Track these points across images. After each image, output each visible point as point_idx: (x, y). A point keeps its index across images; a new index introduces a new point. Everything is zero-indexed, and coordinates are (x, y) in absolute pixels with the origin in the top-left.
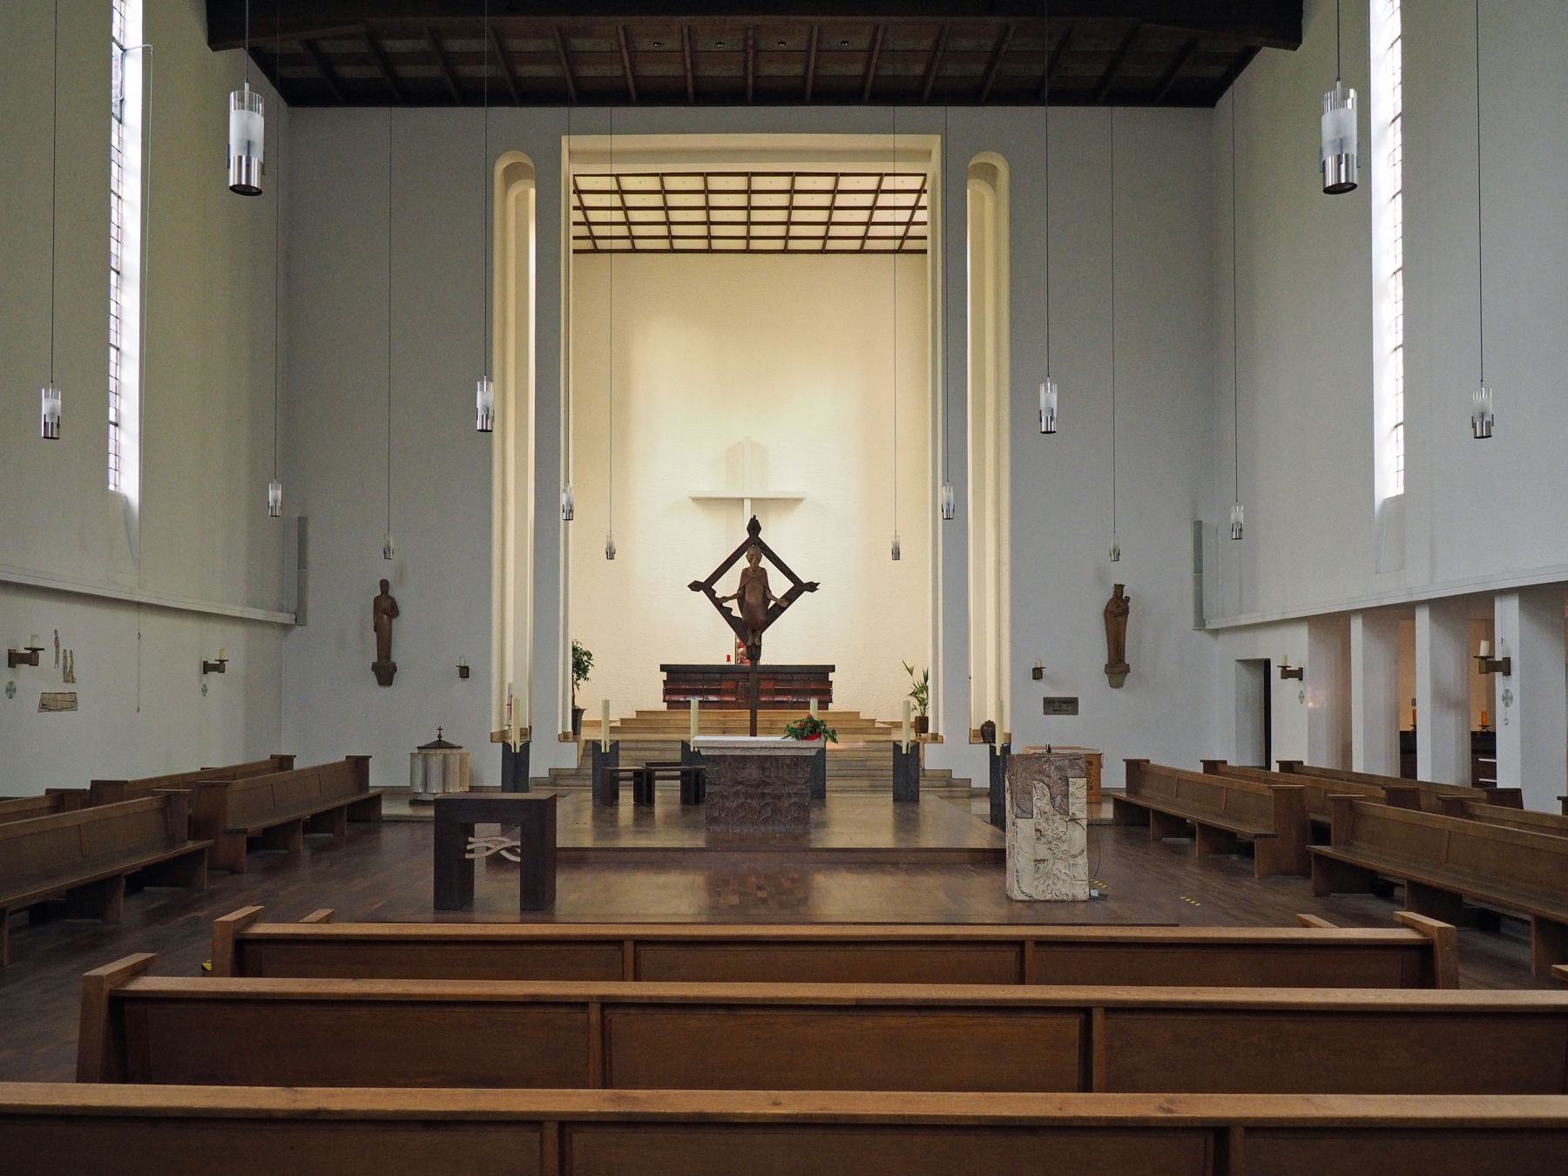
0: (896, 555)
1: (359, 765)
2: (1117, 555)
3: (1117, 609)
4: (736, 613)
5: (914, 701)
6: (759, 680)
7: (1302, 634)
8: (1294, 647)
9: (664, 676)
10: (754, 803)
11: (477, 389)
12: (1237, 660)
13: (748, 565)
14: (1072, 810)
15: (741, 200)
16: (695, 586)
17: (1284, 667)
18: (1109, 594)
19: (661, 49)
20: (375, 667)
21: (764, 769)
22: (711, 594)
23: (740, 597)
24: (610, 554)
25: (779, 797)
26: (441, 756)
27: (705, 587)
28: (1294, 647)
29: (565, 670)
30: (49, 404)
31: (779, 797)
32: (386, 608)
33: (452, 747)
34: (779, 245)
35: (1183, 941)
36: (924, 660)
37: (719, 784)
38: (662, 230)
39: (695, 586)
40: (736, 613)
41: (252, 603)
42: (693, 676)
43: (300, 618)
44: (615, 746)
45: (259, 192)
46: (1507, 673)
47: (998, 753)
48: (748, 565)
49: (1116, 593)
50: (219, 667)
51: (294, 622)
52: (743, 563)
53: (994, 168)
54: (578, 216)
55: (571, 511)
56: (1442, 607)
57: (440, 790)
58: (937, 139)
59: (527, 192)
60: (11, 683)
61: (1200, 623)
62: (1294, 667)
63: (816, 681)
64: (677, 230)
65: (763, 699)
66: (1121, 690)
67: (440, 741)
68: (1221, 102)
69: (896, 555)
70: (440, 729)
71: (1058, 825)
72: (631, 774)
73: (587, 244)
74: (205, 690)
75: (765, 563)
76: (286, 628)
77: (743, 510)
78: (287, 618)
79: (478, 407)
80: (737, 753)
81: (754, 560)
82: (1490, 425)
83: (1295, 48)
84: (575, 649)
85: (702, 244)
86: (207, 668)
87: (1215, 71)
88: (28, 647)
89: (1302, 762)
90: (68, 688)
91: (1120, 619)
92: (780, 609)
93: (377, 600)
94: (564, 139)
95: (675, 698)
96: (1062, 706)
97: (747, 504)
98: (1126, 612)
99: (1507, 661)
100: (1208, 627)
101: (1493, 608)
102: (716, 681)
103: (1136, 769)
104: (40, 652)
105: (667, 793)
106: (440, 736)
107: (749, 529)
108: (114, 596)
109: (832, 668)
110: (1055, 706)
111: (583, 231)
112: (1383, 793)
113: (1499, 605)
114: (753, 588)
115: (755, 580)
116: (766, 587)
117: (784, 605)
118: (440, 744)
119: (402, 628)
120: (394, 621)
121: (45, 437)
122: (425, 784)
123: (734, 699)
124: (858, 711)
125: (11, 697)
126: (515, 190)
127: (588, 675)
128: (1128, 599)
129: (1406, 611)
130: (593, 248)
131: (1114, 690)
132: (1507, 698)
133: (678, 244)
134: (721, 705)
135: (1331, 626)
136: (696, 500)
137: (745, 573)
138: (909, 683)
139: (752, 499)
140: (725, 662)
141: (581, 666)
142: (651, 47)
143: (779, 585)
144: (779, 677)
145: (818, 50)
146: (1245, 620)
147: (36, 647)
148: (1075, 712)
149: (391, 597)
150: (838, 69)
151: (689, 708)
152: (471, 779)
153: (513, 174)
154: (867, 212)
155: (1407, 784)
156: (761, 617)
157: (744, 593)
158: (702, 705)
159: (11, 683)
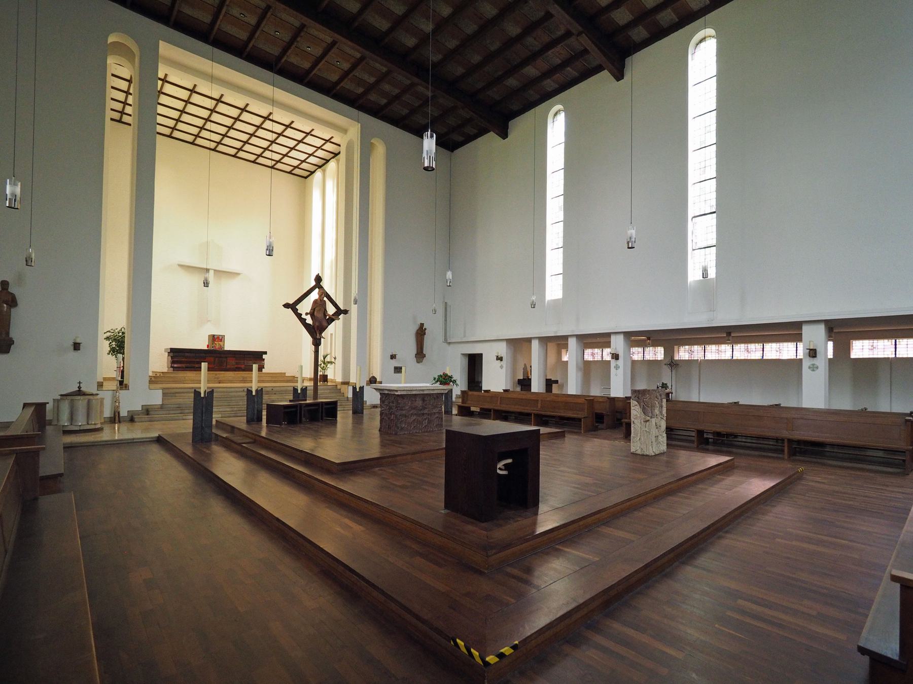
3: (421, 333)
4: (309, 321)
7: (504, 344)
11: (7, 184)
12: (462, 354)
16: (287, 306)
17: (497, 356)
18: (417, 327)
19: (243, 19)
22: (295, 311)
23: (312, 314)
26: (86, 400)
27: (292, 307)
37: (405, 410)
39: (287, 306)
47: (358, 390)
52: (315, 295)
61: (446, 341)
67: (79, 390)
68: (457, 152)
70: (80, 383)
87: (461, 139)
92: (331, 320)
95: (175, 366)
100: (448, 341)
106: (79, 387)
109: (265, 353)
113: (613, 338)
114: (320, 310)
118: (80, 393)
124: (285, 372)
125: (809, 368)
128: (425, 329)
137: (315, 302)
139: (215, 270)
142: (237, 15)
143: (331, 310)
151: (201, 371)
155: (525, 395)
157: (314, 312)
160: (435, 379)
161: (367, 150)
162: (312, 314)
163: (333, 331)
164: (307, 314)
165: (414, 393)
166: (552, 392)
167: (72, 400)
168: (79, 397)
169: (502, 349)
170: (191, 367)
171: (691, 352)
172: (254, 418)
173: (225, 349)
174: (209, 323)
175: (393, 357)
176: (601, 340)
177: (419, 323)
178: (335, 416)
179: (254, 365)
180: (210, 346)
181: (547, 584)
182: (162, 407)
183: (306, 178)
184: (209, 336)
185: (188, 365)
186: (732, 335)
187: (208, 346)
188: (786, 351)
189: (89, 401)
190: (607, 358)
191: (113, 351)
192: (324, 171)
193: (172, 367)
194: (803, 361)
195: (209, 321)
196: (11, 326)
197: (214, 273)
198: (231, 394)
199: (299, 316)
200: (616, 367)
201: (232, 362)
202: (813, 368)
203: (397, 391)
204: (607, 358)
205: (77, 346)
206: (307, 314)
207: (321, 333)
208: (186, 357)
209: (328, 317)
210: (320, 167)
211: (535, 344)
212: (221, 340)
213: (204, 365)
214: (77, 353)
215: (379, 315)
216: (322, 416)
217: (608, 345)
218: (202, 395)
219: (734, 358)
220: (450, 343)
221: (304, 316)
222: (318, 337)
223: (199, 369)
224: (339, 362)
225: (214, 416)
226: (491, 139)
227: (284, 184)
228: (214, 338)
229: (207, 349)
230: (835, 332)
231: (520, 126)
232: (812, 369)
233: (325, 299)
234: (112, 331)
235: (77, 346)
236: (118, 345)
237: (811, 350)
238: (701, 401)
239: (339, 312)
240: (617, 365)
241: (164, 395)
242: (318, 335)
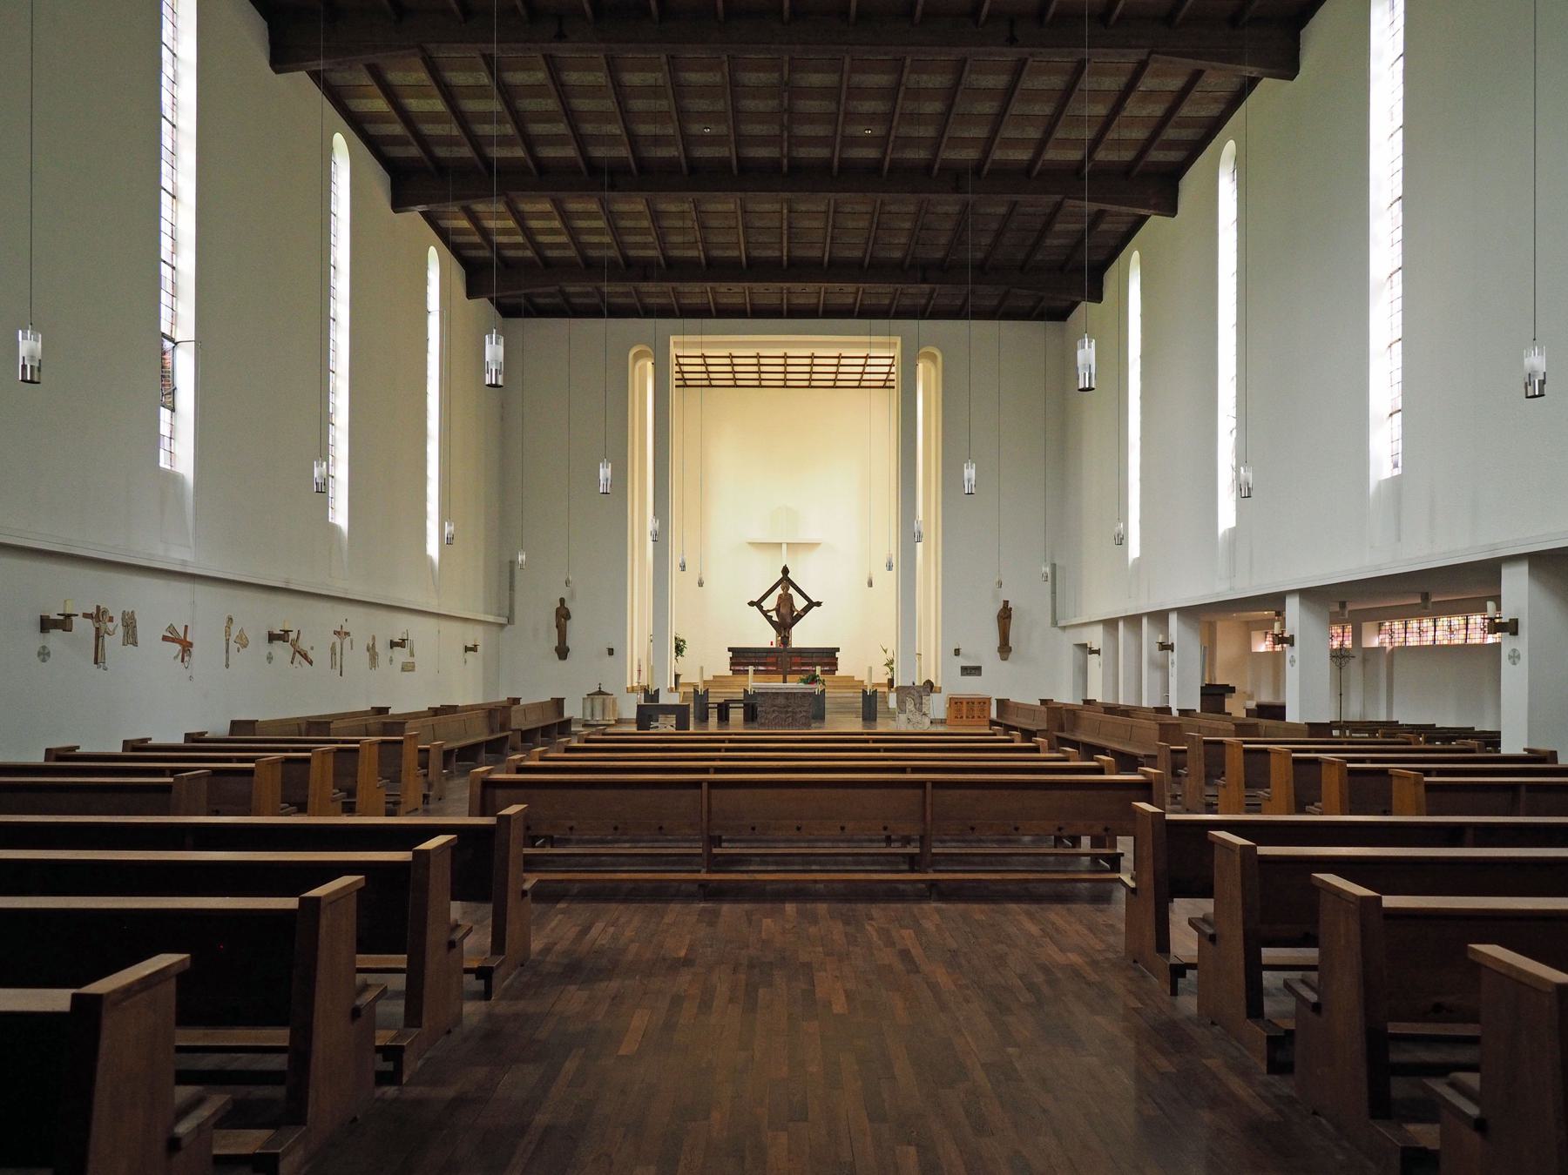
0: (870, 584)
1: (558, 703)
2: (1000, 584)
3: (1005, 615)
4: (775, 618)
5: (888, 669)
6: (791, 657)
7: (1099, 629)
8: (1096, 637)
9: (730, 654)
10: (783, 716)
13: (782, 592)
15: (781, 369)
16: (752, 604)
20: (557, 649)
21: (787, 699)
22: (761, 608)
23: (777, 610)
24: (701, 584)
25: (796, 713)
27: (757, 604)
28: (1096, 637)
29: (671, 650)
30: (28, 346)
31: (796, 713)
32: (563, 615)
33: (608, 694)
34: (806, 383)
36: (891, 645)
38: (730, 376)
39: (752, 604)
40: (775, 618)
41: (486, 613)
42: (750, 654)
43: (510, 620)
44: (707, 691)
45: (501, 386)
48: (782, 592)
50: (474, 649)
51: (506, 622)
52: (779, 591)
53: (935, 356)
54: (677, 369)
55: (684, 566)
56: (1151, 615)
57: (601, 718)
58: (900, 338)
59: (645, 365)
60: (44, 647)
61: (1055, 623)
62: (1096, 648)
63: (828, 657)
64: (738, 376)
65: (793, 668)
69: (870, 584)
72: (716, 705)
73: (681, 383)
74: (270, 658)
75: (791, 591)
76: (502, 626)
78: (503, 620)
79: (601, 478)
80: (774, 691)
81: (785, 589)
82: (1542, 383)
83: (1292, 79)
84: (676, 638)
85: (756, 383)
86: (467, 649)
87: (1174, 156)
88: (62, 612)
89: (1195, 710)
90: (411, 660)
91: (1006, 620)
92: (799, 617)
93: (558, 610)
94: (671, 337)
95: (737, 668)
96: (971, 671)
97: (784, 546)
98: (1009, 617)
99: (1292, 636)
102: (763, 657)
103: (1002, 704)
104: (73, 618)
105: (737, 715)
106: (600, 688)
108: (379, 602)
109: (838, 650)
110: (966, 671)
111: (679, 376)
112: (1233, 727)
114: (785, 605)
115: (786, 600)
116: (792, 605)
117: (802, 614)
118: (600, 693)
119: (573, 627)
120: (568, 622)
121: (22, 380)
122: (592, 715)
123: (775, 668)
125: (44, 661)
126: (640, 363)
127: (683, 654)
130: (684, 384)
133: (739, 383)
134: (767, 672)
135: (1110, 624)
136: (750, 543)
137: (780, 597)
138: (884, 659)
140: (769, 646)
141: (679, 649)
143: (799, 603)
144: (803, 655)
145: (835, 212)
146: (1075, 621)
147: (68, 612)
148: (980, 674)
149: (567, 609)
150: (847, 254)
152: (619, 714)
153: (637, 357)
154: (864, 360)
156: (789, 620)
158: (756, 672)
159: (270, 653)
166: (1284, 719)
167: (592, 699)
181: (765, 837)
186: (1434, 600)
205: (611, 652)
209: (796, 613)
219: (1437, 643)
220: (1064, 628)
230: (1435, 602)
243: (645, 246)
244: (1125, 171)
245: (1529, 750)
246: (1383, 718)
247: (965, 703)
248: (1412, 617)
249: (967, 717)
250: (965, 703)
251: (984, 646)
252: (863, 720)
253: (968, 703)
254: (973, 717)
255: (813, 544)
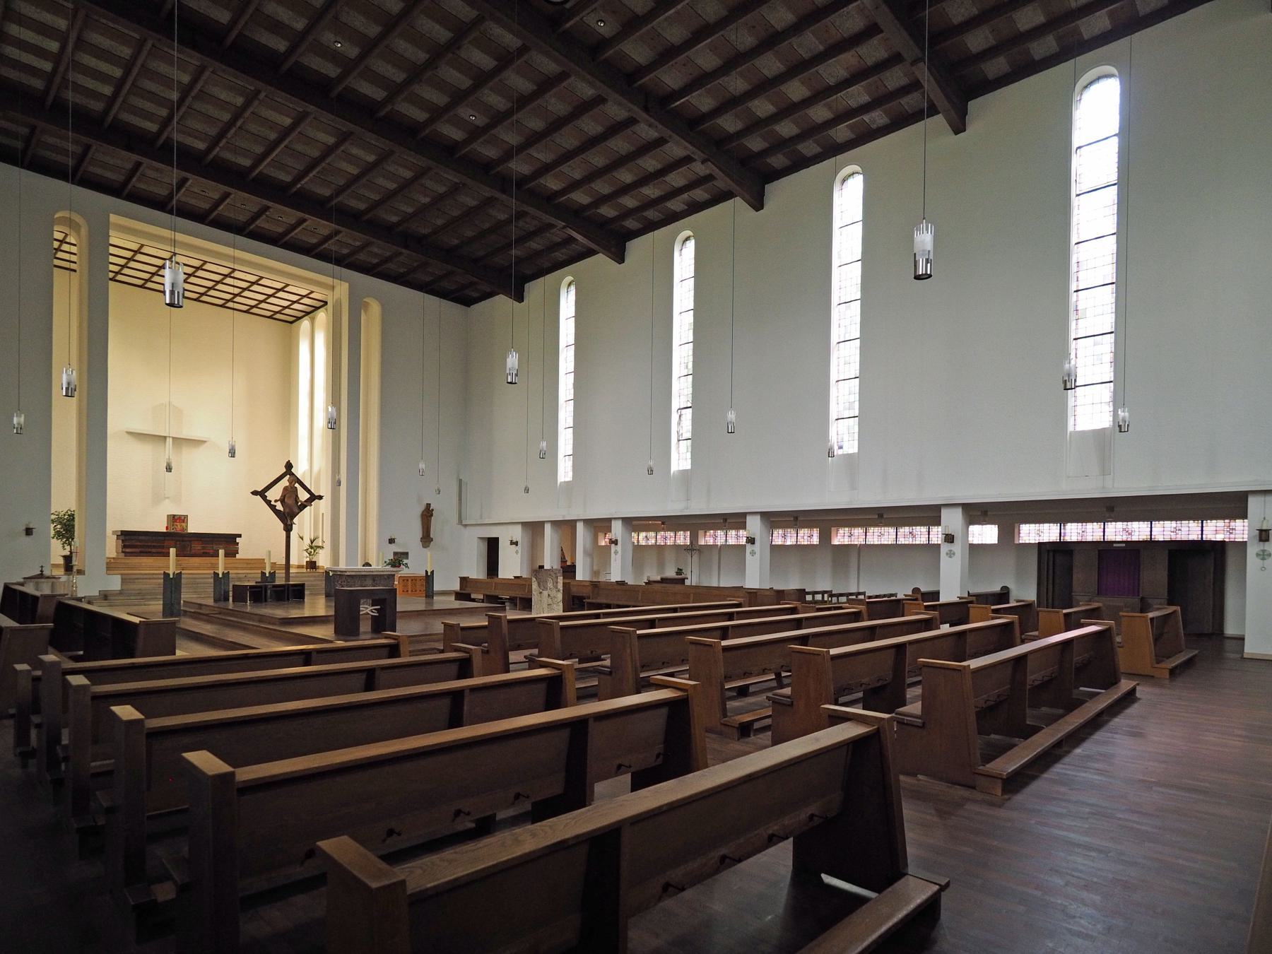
3: (427, 514)
4: (279, 507)
7: (519, 528)
13: (287, 484)
14: (559, 587)
16: (255, 493)
17: (611, 539)
18: (423, 508)
22: (264, 498)
23: (282, 500)
26: (50, 584)
27: (261, 494)
35: (338, 671)
39: (255, 493)
46: (616, 544)
48: (287, 484)
49: (427, 507)
52: (285, 482)
61: (460, 522)
66: (428, 548)
67: (42, 574)
70: (42, 567)
71: (553, 593)
77: (165, 447)
83: (757, 211)
87: (475, 295)
92: (303, 507)
95: (127, 550)
97: (169, 441)
99: (617, 540)
100: (463, 523)
101: (611, 523)
106: (42, 571)
107: (285, 467)
109: (240, 536)
113: (749, 519)
125: (947, 554)
128: (433, 510)
129: (541, 524)
131: (425, 549)
132: (616, 552)
137: (285, 489)
139: (173, 438)
142: (198, 192)
143: (304, 495)
160: (385, 562)
161: (357, 307)
162: (282, 500)
163: (304, 521)
164: (276, 501)
165: (363, 573)
167: (37, 583)
168: (43, 580)
169: (517, 533)
170: (158, 553)
171: (715, 537)
172: (221, 597)
173: (189, 531)
174: (167, 500)
175: (392, 541)
176: (735, 520)
177: (425, 503)
178: (304, 598)
179: (220, 551)
180: (169, 526)
182: (121, 593)
183: (291, 323)
184: (168, 516)
185: (143, 550)
187: (167, 528)
188: (920, 535)
189: (53, 584)
190: (743, 541)
191: (59, 535)
192: (313, 321)
193: (123, 552)
194: (942, 547)
195: (168, 498)
196: (1076, 711)
197: (173, 441)
198: (198, 580)
199: (268, 502)
200: (950, 554)
201: (197, 547)
202: (951, 554)
203: (346, 572)
204: (743, 541)
205: (29, 531)
206: (276, 501)
207: (292, 519)
208: (140, 541)
209: (300, 503)
210: (307, 313)
211: (548, 528)
212: (184, 522)
213: (172, 551)
214: (29, 539)
215: (375, 495)
216: (288, 596)
217: (743, 526)
218: (171, 576)
220: (466, 526)
221: (273, 503)
222: (289, 523)
223: (168, 555)
224: (327, 546)
225: (182, 596)
226: (502, 303)
227: (260, 333)
228: (174, 519)
229: (165, 531)
231: (534, 289)
232: (1261, 557)
233: (297, 485)
234: (56, 513)
235: (29, 531)
236: (67, 529)
237: (947, 535)
238: (721, 586)
239: (313, 497)
240: (1264, 551)
241: (123, 581)
242: (289, 521)
243: (148, 116)
244: (604, 223)
245: (960, 598)
246: (715, 585)
247: (410, 580)
248: (732, 529)
249: (412, 591)
250: (410, 580)
251: (410, 538)
252: (326, 596)
253: (412, 580)
254: (416, 591)
255: (199, 441)
